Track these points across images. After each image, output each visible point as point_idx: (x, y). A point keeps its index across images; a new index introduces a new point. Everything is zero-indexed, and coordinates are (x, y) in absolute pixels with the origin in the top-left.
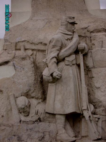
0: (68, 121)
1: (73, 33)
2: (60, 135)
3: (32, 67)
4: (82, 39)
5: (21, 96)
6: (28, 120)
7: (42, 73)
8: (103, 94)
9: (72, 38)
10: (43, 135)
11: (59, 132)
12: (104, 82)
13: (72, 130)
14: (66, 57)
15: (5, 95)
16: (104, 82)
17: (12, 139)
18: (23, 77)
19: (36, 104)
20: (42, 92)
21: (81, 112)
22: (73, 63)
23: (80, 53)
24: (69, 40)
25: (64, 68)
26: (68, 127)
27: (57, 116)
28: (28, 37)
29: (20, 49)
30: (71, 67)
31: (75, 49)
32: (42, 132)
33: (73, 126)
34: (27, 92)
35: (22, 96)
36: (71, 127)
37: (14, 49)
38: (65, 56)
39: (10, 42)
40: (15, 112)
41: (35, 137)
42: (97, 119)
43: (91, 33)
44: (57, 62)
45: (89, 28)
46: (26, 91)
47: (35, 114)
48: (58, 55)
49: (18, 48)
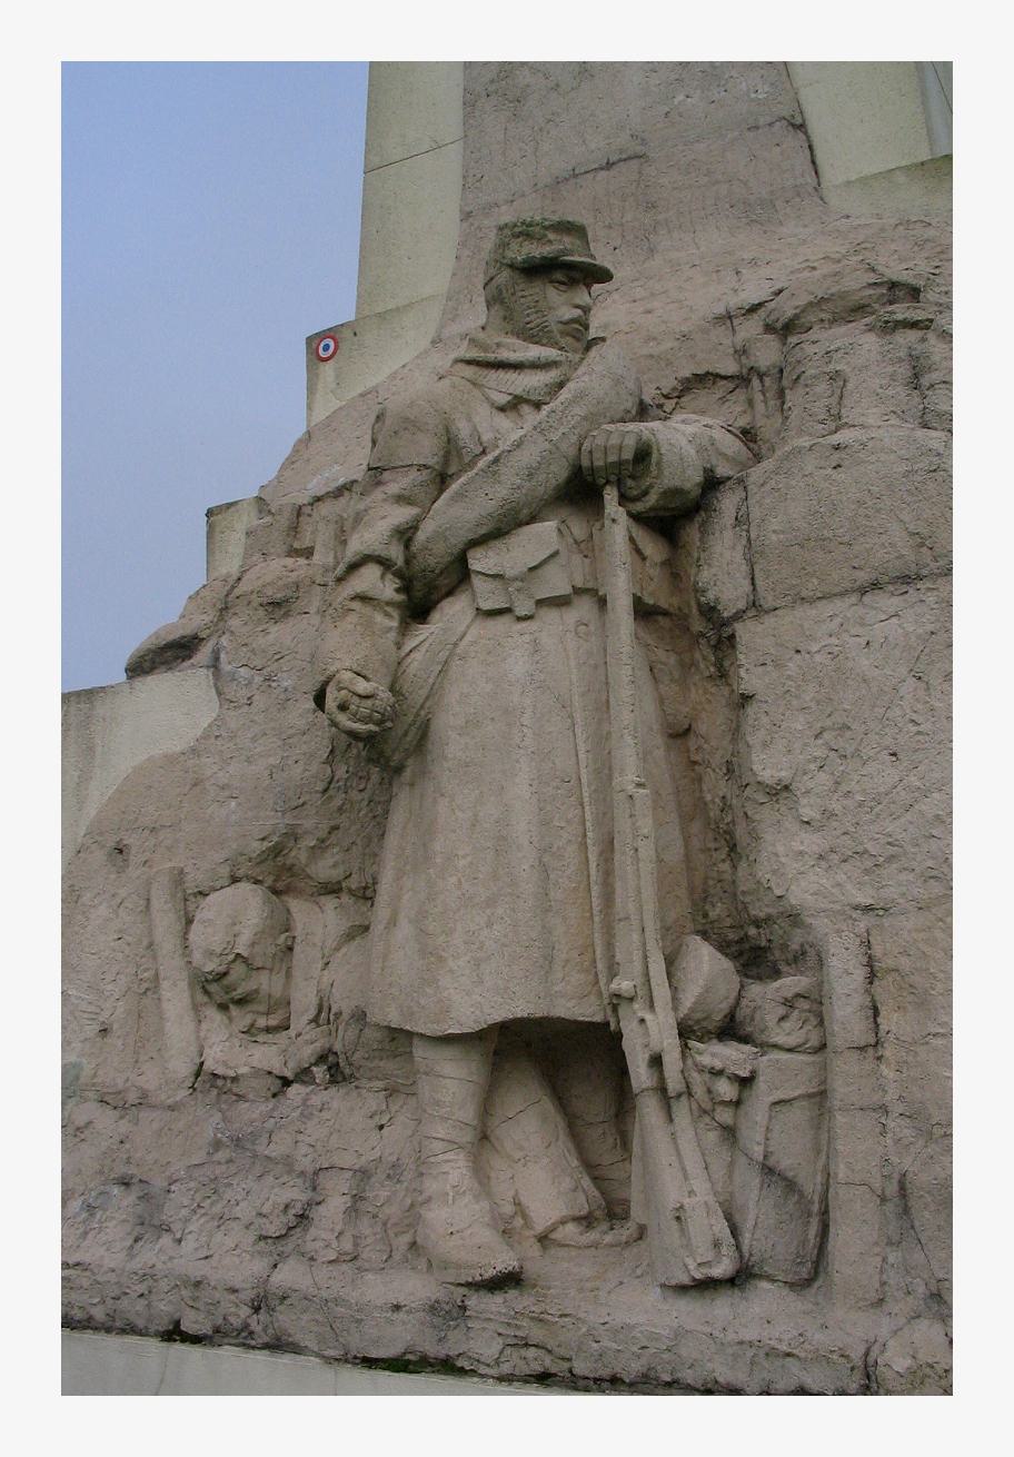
4: (723, 400)
5: (235, 880)
6: (243, 1070)
8: (811, 842)
10: (304, 1197)
12: (823, 730)
14: (475, 543)
15: (138, 878)
16: (823, 730)
18: (254, 739)
23: (610, 496)
25: (468, 638)
32: (302, 1174)
34: (277, 851)
38: (457, 540)
40: (176, 998)
42: (726, 1089)
46: (266, 844)
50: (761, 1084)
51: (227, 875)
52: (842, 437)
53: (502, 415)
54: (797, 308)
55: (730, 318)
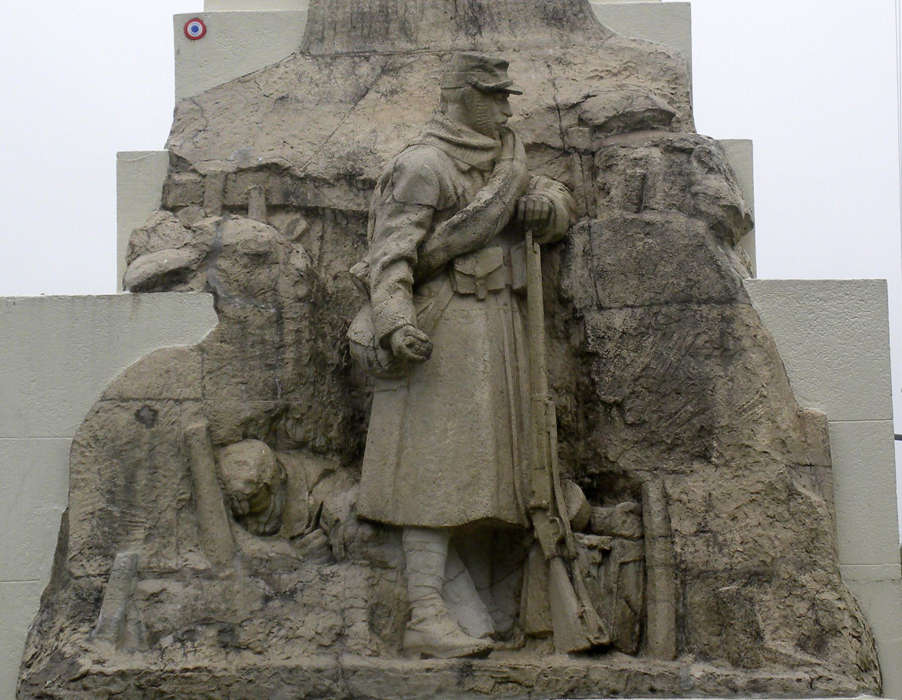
0: (466, 564)
1: (501, 137)
2: (419, 627)
3: (300, 300)
7: (348, 325)
8: (628, 434)
9: (493, 163)
11: (415, 612)
13: (484, 606)
17: (193, 641)
19: (314, 478)
20: (344, 419)
21: (525, 518)
22: (492, 288)
23: (529, 236)
24: (476, 175)
26: (463, 588)
27: (411, 538)
28: (287, 147)
29: (243, 209)
30: (480, 305)
31: (506, 219)
33: (491, 585)
35: (391, 171)
36: (477, 589)
37: (217, 204)
39: (194, 171)
41: (299, 632)
43: (595, 132)
44: (412, 280)
45: (586, 106)
47: (308, 527)
48: (421, 246)
49: (236, 199)
50: (615, 553)
51: (241, 433)
52: (648, 216)
53: (463, 176)
54: (607, 117)
55: (558, 110)
